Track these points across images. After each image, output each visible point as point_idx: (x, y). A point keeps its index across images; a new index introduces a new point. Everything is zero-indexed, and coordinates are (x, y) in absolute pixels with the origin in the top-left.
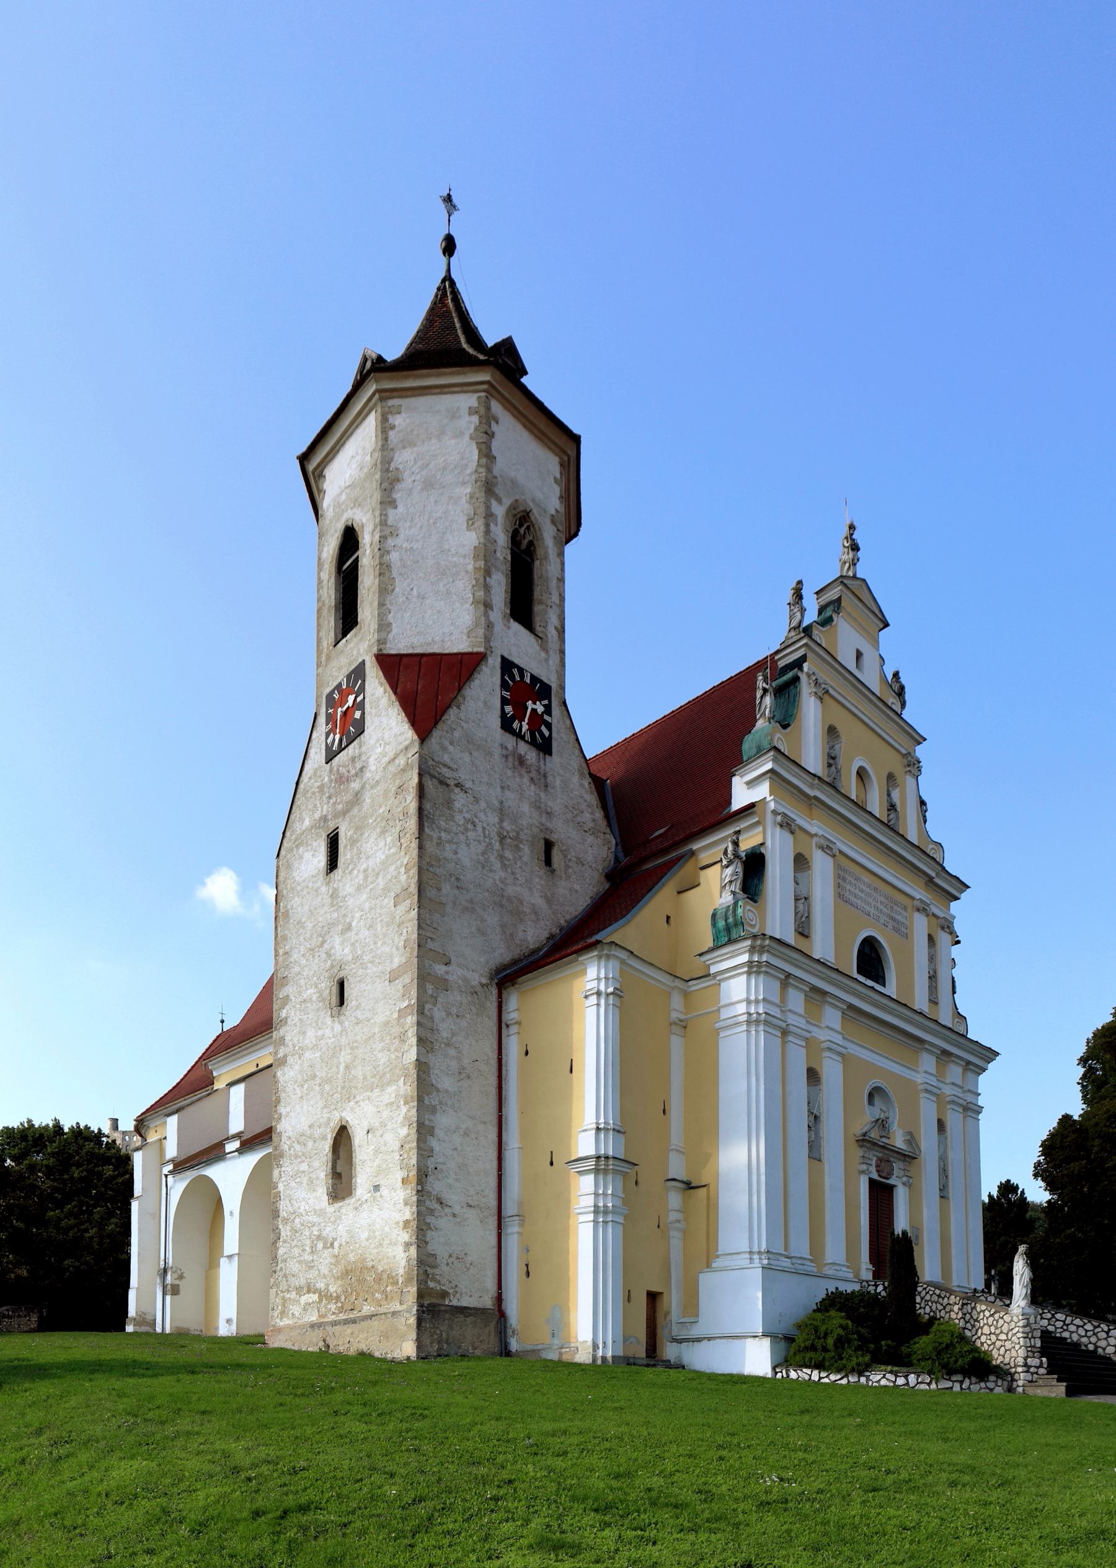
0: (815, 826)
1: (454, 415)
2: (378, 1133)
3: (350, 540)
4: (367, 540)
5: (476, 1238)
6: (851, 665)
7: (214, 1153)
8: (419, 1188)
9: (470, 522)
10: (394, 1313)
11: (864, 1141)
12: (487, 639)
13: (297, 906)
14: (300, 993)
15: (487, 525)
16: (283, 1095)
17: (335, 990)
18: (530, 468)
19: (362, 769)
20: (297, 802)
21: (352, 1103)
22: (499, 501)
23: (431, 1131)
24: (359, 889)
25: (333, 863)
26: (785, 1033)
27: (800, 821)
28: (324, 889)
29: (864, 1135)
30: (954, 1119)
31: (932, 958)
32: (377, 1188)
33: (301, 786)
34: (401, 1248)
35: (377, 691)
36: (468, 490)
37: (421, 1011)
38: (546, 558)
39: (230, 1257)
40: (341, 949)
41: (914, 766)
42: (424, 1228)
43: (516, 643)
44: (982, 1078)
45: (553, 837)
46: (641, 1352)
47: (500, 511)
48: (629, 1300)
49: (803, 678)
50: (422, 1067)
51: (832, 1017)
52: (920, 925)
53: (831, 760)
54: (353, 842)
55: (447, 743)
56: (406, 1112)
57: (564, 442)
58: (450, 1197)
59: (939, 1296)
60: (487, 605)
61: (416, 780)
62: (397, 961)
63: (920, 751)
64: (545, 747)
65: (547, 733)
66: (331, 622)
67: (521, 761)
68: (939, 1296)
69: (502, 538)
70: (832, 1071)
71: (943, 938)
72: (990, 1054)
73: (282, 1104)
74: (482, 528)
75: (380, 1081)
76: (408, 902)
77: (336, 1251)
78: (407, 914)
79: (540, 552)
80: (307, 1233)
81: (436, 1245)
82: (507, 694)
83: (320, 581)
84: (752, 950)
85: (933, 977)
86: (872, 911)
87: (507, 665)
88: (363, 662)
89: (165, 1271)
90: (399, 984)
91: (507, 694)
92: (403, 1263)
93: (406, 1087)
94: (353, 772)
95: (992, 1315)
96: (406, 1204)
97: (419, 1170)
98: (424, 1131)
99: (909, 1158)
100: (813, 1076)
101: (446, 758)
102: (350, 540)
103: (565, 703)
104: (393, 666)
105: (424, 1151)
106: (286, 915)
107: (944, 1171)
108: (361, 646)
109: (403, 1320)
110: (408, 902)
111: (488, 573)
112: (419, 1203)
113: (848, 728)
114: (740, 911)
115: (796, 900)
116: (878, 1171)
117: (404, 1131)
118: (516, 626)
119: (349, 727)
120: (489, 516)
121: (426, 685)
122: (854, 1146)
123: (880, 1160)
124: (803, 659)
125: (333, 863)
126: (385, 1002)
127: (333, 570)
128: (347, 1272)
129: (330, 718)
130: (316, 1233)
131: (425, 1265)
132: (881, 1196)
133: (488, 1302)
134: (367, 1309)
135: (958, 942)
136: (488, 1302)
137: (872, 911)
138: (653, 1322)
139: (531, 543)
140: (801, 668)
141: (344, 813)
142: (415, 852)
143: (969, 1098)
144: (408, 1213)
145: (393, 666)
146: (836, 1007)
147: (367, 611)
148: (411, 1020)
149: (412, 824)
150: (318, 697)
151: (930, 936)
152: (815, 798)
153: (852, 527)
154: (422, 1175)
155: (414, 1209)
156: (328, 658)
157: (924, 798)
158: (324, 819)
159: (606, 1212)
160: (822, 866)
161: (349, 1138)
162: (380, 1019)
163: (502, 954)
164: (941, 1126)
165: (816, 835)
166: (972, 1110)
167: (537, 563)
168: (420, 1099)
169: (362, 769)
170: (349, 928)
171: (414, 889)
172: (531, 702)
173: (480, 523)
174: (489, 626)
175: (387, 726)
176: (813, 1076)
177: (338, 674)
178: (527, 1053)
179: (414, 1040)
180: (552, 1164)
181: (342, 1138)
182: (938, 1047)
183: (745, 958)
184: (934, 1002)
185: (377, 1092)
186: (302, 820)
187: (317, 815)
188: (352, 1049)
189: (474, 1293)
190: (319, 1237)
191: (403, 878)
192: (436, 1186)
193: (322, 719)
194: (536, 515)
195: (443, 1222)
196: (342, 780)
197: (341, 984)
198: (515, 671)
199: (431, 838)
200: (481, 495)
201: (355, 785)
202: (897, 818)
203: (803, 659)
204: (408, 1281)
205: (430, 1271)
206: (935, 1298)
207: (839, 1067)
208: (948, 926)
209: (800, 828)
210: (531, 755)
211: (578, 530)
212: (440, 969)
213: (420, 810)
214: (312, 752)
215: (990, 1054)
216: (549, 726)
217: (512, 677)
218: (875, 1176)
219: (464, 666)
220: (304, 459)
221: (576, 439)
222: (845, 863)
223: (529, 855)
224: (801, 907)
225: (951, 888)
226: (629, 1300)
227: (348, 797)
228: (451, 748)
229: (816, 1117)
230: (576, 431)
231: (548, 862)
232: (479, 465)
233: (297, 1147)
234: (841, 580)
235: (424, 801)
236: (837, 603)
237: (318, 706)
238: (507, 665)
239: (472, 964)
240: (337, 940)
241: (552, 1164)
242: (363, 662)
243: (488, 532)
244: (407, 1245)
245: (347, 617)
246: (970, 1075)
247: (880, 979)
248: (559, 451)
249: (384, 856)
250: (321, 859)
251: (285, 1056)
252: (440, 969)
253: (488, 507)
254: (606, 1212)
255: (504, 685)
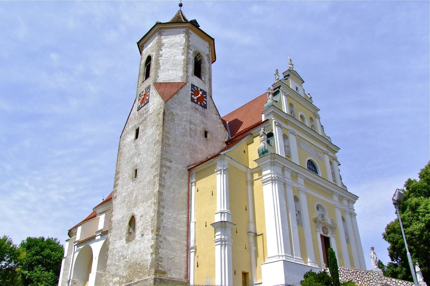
0: (289, 127)
2: (144, 217)
3: (149, 59)
4: (153, 58)
6: (295, 90)
7: (92, 239)
8: (157, 233)
9: (183, 54)
10: (145, 280)
11: (315, 221)
12: (187, 79)
13: (124, 150)
14: (123, 176)
15: (187, 55)
16: (114, 208)
17: (134, 173)
18: (203, 47)
19: (147, 111)
20: (128, 122)
21: (136, 208)
22: (191, 50)
23: (162, 214)
24: (144, 143)
25: (137, 137)
26: (285, 184)
27: (283, 125)
29: (316, 218)
30: (348, 217)
31: (332, 168)
32: (142, 235)
33: (130, 118)
34: (149, 256)
35: (153, 92)
36: (182, 47)
37: (161, 176)
38: (205, 63)
40: (137, 160)
41: (317, 117)
42: (158, 247)
43: (195, 81)
44: (355, 205)
45: (207, 130)
47: (191, 52)
48: (235, 274)
49: (281, 91)
50: (160, 193)
51: (301, 181)
52: (327, 159)
53: (292, 112)
54: (143, 130)
55: (173, 103)
56: (154, 207)
57: (211, 40)
59: (348, 270)
60: (187, 72)
61: (163, 111)
62: (154, 162)
63: (319, 112)
64: (205, 107)
65: (205, 103)
66: (143, 77)
67: (197, 109)
68: (348, 270)
69: (192, 58)
70: (303, 198)
71: (335, 163)
72: (356, 198)
73: (114, 211)
74: (186, 55)
75: (146, 199)
76: (158, 145)
77: (127, 260)
78: (158, 147)
79: (203, 62)
80: (118, 255)
82: (193, 93)
83: (140, 69)
84: (271, 158)
85: (333, 174)
86: (310, 152)
87: (193, 86)
88: (150, 85)
89: (69, 281)
90: (154, 168)
91: (193, 93)
92: (150, 261)
93: (154, 200)
94: (145, 112)
95: (366, 274)
96: (152, 239)
97: (157, 227)
98: (159, 214)
99: (334, 228)
100: (296, 199)
101: (173, 106)
102: (149, 59)
103: (211, 97)
104: (159, 86)
106: (121, 153)
107: (347, 234)
108: (150, 81)
109: (149, 282)
110: (158, 145)
111: (187, 64)
112: (157, 239)
113: (295, 105)
114: (266, 147)
115: (285, 146)
116: (323, 232)
117: (153, 215)
118: (196, 77)
119: (144, 100)
120: (188, 53)
121: (168, 91)
122: (313, 223)
123: (323, 227)
124: (280, 86)
125: (137, 137)
126: (149, 175)
127: (144, 65)
128: (130, 266)
129: (139, 100)
130: (121, 254)
132: (326, 241)
134: (136, 280)
135: (340, 165)
137: (310, 152)
139: (200, 60)
140: (279, 88)
141: (141, 123)
142: (162, 130)
143: (352, 211)
144: (153, 242)
145: (159, 86)
146: (302, 178)
147: (152, 73)
148: (157, 179)
149: (161, 123)
150: (137, 95)
151: (330, 162)
152: (287, 120)
153: (291, 60)
155: (155, 240)
156: (141, 85)
157: (322, 125)
158: (135, 125)
159: (225, 241)
160: (292, 139)
161: (135, 220)
162: (147, 180)
164: (343, 220)
165: (289, 130)
166: (353, 215)
167: (202, 65)
168: (159, 203)
169: (147, 111)
170: (139, 155)
171: (160, 140)
172: (201, 99)
173: (186, 54)
174: (187, 76)
175: (156, 101)
176: (296, 199)
177: (143, 88)
178: (198, 191)
179: (158, 185)
180: (206, 226)
182: (338, 194)
183: (269, 160)
184: (335, 181)
185: (145, 203)
186: (129, 126)
187: (133, 125)
188: (138, 190)
190: (122, 256)
191: (157, 138)
193: (137, 100)
194: (202, 54)
196: (142, 115)
197: (136, 171)
198: (195, 87)
199: (167, 127)
200: (186, 48)
201: (145, 115)
202: (314, 128)
203: (280, 86)
204: (151, 267)
205: (160, 263)
206: (347, 271)
207: (305, 196)
208: (335, 159)
209: (284, 127)
210: (200, 108)
211: (216, 59)
212: (168, 164)
213: (164, 119)
214: (134, 108)
215: (356, 198)
216: (206, 102)
217: (194, 89)
218: (322, 233)
219: (181, 86)
220: (138, 43)
221: (213, 40)
222: (299, 138)
224: (287, 149)
225: (335, 149)
226: (235, 274)
227: (143, 118)
228: (174, 104)
229: (298, 212)
230: (213, 38)
231: (206, 136)
232: (185, 42)
233: (117, 225)
234: (289, 70)
236: (288, 75)
237: (137, 97)
238: (193, 86)
240: (136, 158)
241: (206, 226)
242: (150, 85)
243: (187, 56)
244: (152, 254)
245: (147, 75)
246: (350, 203)
247: (316, 172)
248: (209, 42)
249: (152, 132)
250: (134, 136)
251: (116, 196)
252: (168, 164)
253: (188, 51)
254: (225, 241)
255: (192, 90)
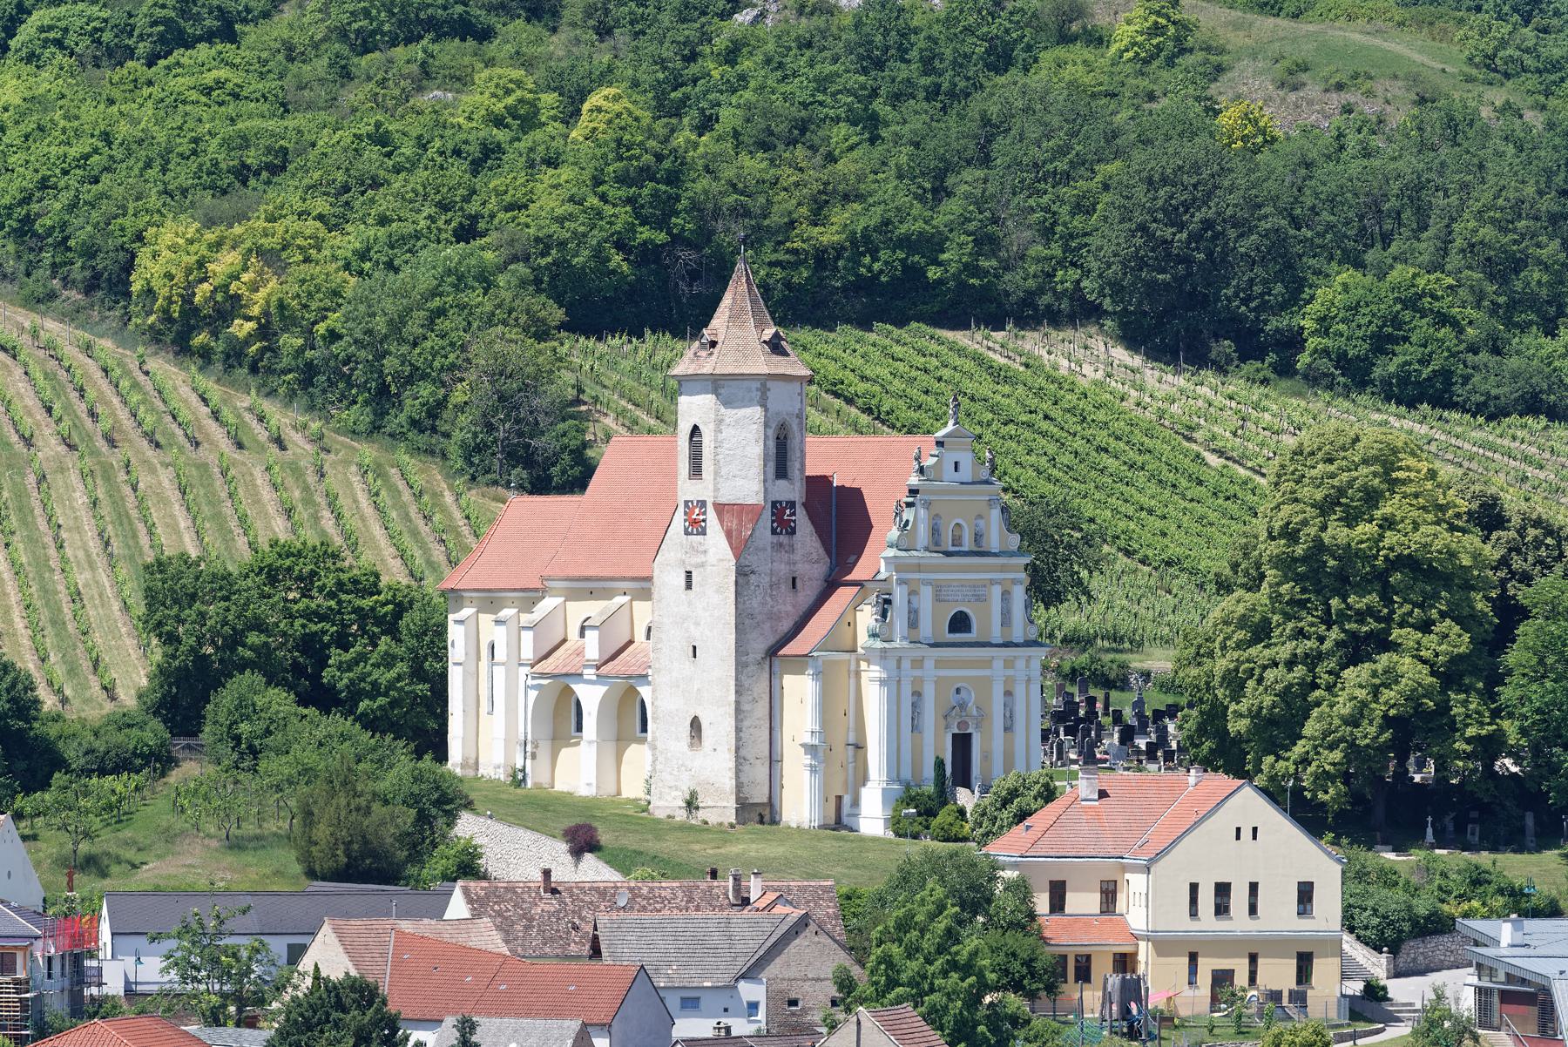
1: (750, 390)
5: (760, 772)
28: (549, 129)
39: (590, 742)
46: (1533, 1011)
58: (748, 756)
67: (781, 545)
81: (743, 779)
105: (738, 739)
131: (739, 787)
133: (765, 800)
136: (765, 800)
138: (839, 821)
154: (737, 749)
163: (772, 640)
181: (648, 638)
189: (759, 795)
192: (743, 752)
195: (746, 768)
223: (785, 588)
235: (743, 699)
239: (759, 646)
